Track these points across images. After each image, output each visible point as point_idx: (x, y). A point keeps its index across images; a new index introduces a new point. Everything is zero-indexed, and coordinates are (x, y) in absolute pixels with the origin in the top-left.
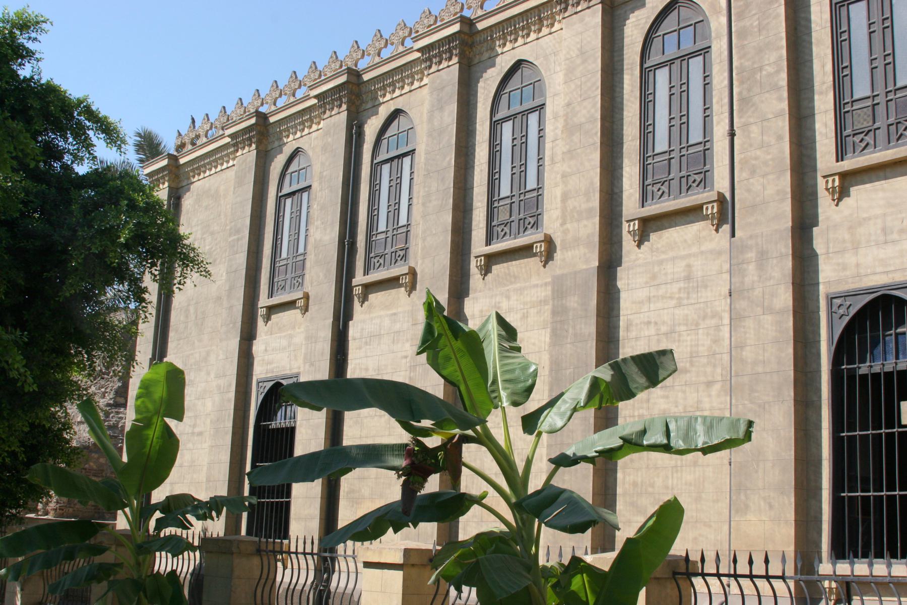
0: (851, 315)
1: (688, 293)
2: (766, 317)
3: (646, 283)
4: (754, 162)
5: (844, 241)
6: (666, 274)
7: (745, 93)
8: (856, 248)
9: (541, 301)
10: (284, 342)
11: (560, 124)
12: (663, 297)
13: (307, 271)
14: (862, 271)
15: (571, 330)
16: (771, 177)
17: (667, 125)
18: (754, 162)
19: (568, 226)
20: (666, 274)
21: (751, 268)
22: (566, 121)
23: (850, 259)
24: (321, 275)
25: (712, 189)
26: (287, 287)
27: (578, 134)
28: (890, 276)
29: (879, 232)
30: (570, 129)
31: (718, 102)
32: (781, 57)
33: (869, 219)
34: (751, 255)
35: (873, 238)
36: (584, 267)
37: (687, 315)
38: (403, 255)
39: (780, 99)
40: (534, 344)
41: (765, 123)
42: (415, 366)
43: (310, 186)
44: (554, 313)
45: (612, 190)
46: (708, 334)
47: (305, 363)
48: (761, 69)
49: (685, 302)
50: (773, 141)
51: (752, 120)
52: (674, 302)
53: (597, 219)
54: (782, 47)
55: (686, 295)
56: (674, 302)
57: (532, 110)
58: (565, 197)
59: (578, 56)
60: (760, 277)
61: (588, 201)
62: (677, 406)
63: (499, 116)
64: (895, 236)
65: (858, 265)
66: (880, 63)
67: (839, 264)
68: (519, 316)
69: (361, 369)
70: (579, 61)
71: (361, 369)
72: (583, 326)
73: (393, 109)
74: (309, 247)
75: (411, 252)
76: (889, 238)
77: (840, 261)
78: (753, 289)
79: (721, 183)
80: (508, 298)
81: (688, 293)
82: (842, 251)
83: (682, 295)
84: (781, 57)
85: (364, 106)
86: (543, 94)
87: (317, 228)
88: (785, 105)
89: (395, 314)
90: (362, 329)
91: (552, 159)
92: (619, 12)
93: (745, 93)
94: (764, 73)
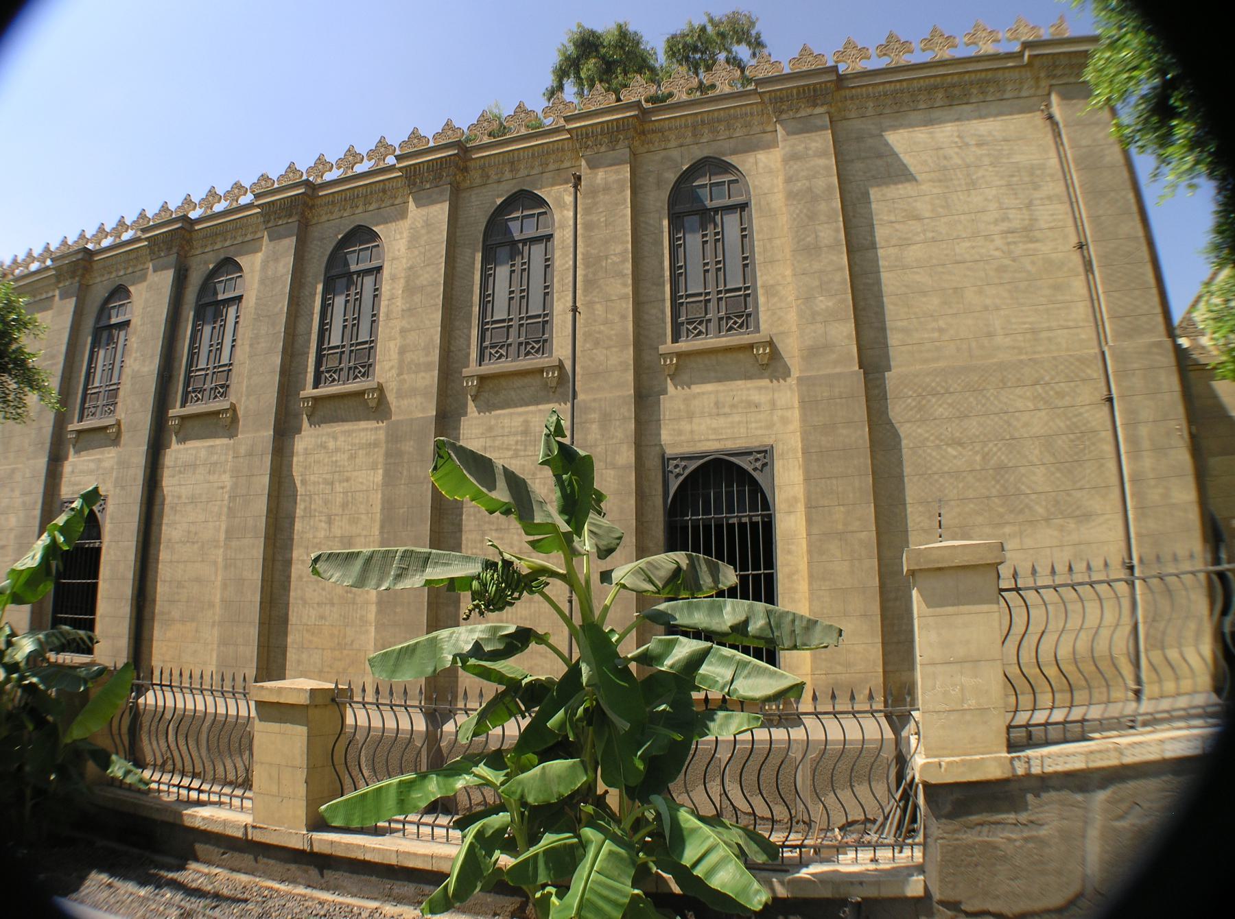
0: (685, 474)
1: (526, 446)
2: (608, 471)
3: (482, 434)
4: (598, 336)
5: (679, 410)
6: (503, 427)
7: (590, 276)
8: (691, 417)
9: (370, 444)
10: (92, 466)
11: (401, 283)
12: (499, 448)
13: (120, 400)
14: (697, 438)
15: (405, 473)
16: (614, 350)
17: (507, 296)
18: (598, 336)
19: (405, 376)
20: (503, 427)
21: (594, 427)
22: (407, 282)
23: (685, 426)
24: (137, 404)
25: (551, 355)
26: (98, 413)
27: (419, 295)
28: (722, 443)
29: (712, 405)
30: (410, 290)
31: (559, 282)
32: (626, 250)
33: (703, 393)
34: (594, 416)
35: (706, 410)
36: (421, 415)
37: (524, 466)
38: (223, 390)
39: (625, 285)
40: (362, 483)
41: (609, 303)
42: (235, 497)
43: (240, 298)
44: (388, 455)
45: (449, 347)
46: (545, 484)
47: (115, 487)
48: (607, 258)
49: (522, 453)
50: (617, 319)
51: (597, 300)
52: (511, 453)
53: (436, 373)
54: (627, 242)
55: (523, 448)
56: (511, 453)
57: (368, 272)
58: (402, 351)
59: (423, 227)
60: (603, 436)
61: (427, 355)
62: (512, 547)
63: (334, 272)
64: (727, 410)
65: (692, 432)
66: (517, 295)
67: (674, 430)
68: (346, 456)
69: (173, 496)
70: (423, 231)
71: (173, 496)
72: (418, 469)
73: (222, 257)
74: (124, 377)
75: (232, 389)
76: (722, 411)
77: (676, 427)
78: (596, 446)
79: (560, 349)
80: (335, 438)
81: (526, 446)
82: (679, 419)
83: (519, 447)
84: (626, 250)
85: (193, 252)
86: (379, 257)
87: (135, 360)
88: (629, 290)
89: (212, 446)
90: (176, 459)
91: (387, 315)
92: (463, 195)
93: (590, 276)
94: (609, 261)
